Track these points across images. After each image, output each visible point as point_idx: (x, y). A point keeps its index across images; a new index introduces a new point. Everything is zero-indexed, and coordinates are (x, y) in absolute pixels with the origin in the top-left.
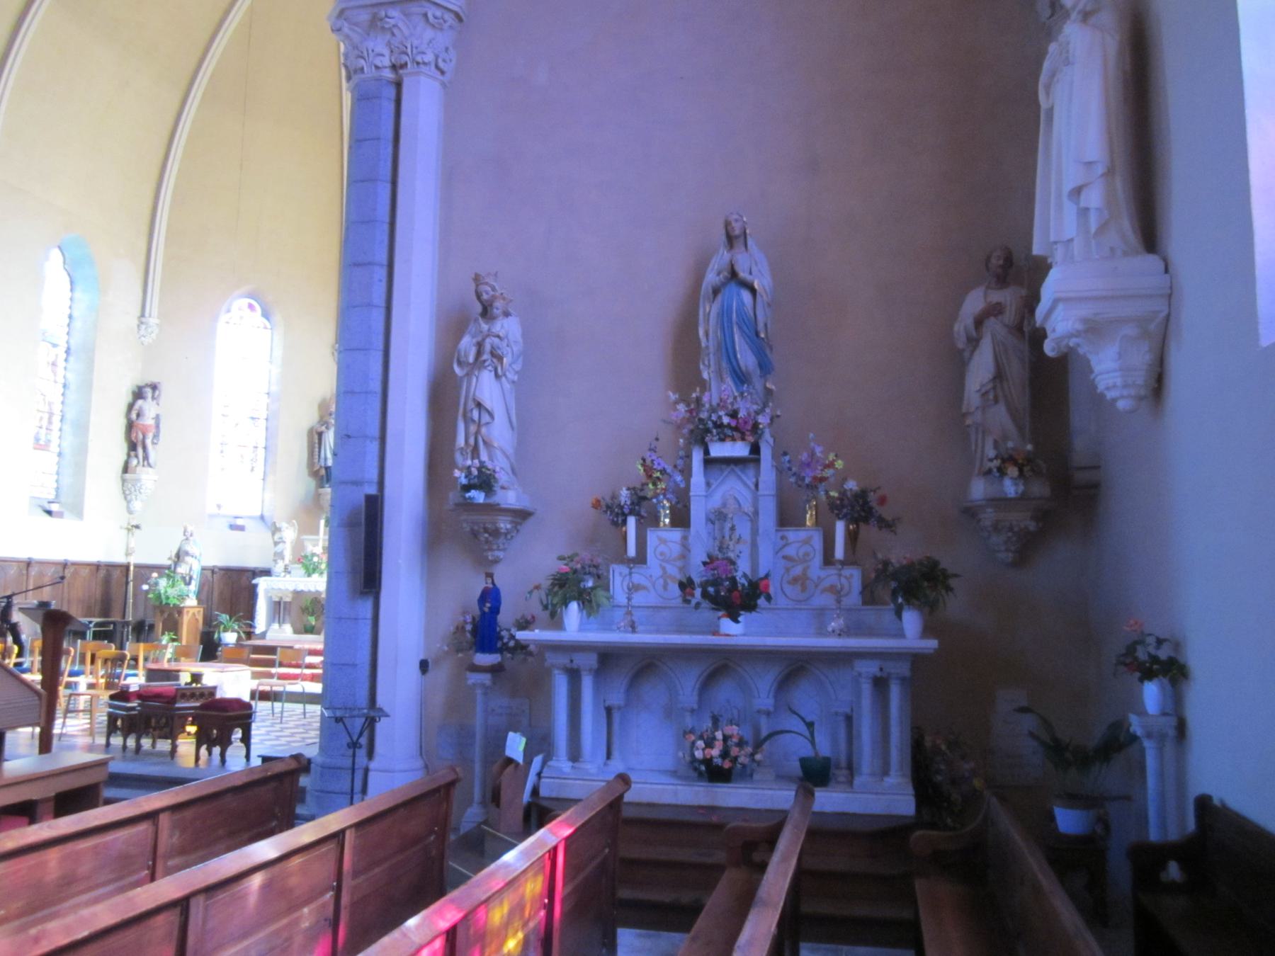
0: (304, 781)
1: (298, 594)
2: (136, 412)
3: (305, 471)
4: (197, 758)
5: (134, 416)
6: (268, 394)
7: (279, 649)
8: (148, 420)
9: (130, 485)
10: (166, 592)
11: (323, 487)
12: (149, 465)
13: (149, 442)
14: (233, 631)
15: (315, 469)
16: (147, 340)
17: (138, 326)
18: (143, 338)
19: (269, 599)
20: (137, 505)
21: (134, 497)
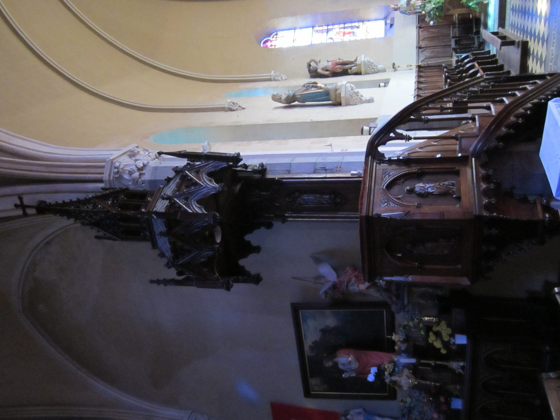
2: (324, 71)
5: (327, 73)
6: (313, 27)
12: (356, 60)
17: (276, 81)
20: (380, 66)
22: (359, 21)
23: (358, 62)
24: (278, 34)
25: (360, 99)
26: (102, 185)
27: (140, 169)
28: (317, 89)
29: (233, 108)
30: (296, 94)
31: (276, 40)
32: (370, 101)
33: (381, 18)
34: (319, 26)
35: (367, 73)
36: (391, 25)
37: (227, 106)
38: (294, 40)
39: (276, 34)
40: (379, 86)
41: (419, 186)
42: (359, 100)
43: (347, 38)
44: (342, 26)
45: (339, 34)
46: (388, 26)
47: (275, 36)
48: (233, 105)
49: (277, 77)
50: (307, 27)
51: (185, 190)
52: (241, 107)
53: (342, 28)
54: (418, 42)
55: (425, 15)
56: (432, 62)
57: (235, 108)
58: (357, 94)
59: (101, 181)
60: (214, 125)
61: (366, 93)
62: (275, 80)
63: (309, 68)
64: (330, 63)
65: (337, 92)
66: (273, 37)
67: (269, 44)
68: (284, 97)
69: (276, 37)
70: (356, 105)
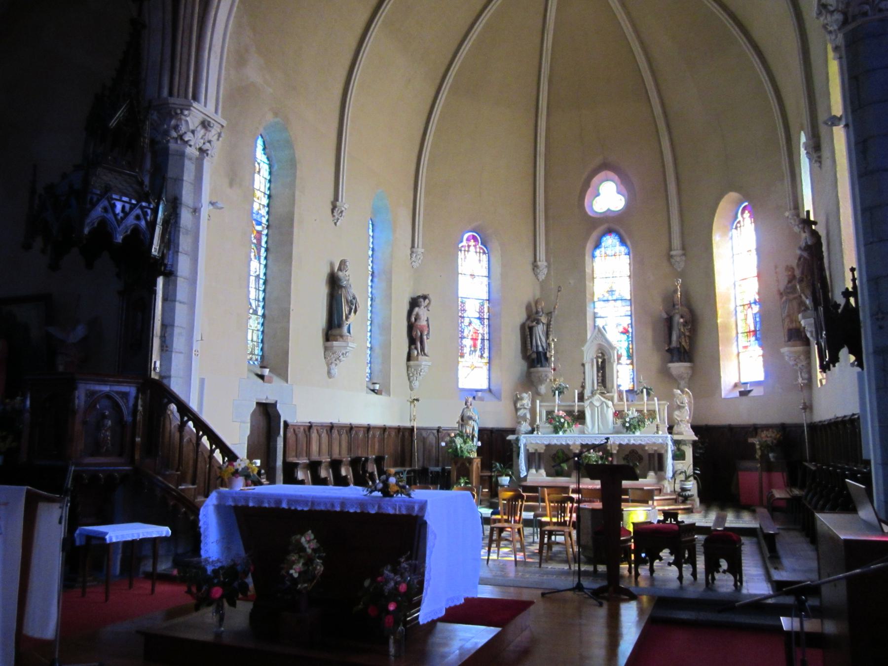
1: (548, 446)
4: (680, 578)
5: (413, 319)
6: (488, 300)
7: (630, 490)
8: (423, 322)
9: (413, 370)
10: (461, 447)
11: (534, 367)
12: (425, 354)
13: (425, 337)
14: (507, 475)
15: (528, 354)
16: (416, 265)
17: (411, 254)
18: (413, 263)
19: (527, 451)
20: (416, 384)
21: (415, 378)
22: (490, 358)
24: (484, 255)
25: (332, 363)
27: (181, 137)
28: (346, 314)
29: (335, 212)
30: (344, 290)
31: (476, 252)
33: (491, 385)
34: (489, 308)
37: (338, 204)
38: (473, 275)
39: (484, 253)
42: (330, 361)
43: (468, 342)
44: (486, 337)
45: (475, 333)
47: (482, 251)
48: (339, 211)
49: (415, 255)
52: (337, 221)
53: (484, 337)
57: (335, 214)
59: (171, 94)
60: (297, 193)
63: (422, 297)
65: (339, 337)
66: (481, 248)
69: (480, 253)
70: (325, 358)
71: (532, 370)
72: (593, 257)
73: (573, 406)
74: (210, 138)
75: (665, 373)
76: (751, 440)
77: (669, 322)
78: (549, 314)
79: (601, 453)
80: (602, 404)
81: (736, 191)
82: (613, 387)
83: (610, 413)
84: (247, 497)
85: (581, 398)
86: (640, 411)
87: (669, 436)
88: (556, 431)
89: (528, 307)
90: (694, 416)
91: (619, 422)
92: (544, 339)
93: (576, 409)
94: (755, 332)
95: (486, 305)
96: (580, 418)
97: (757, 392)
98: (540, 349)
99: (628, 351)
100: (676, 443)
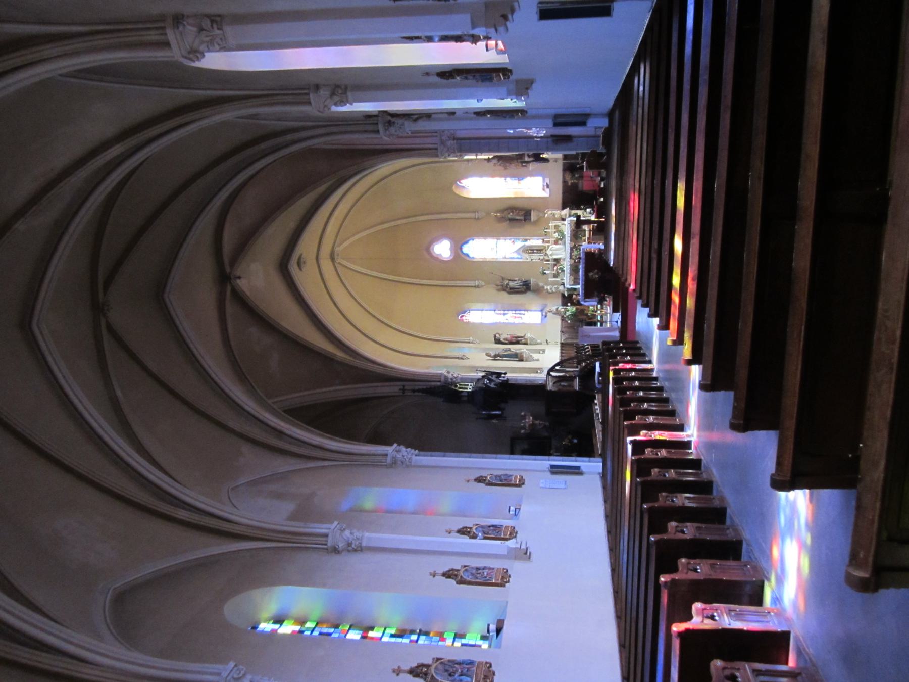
0: (656, 321)
3: (524, 295)
20: (539, 341)
22: (524, 311)
23: (526, 338)
26: (439, 384)
27: (455, 378)
32: (538, 360)
34: (499, 311)
35: (531, 344)
36: (546, 316)
37: (460, 356)
39: (469, 312)
40: (540, 353)
41: (562, 384)
43: (517, 321)
44: (514, 312)
46: (544, 317)
50: (490, 310)
51: (621, 345)
54: (562, 329)
55: (565, 318)
56: (569, 341)
58: (531, 356)
61: (535, 356)
62: (472, 343)
64: (509, 336)
67: (464, 318)
68: (493, 355)
71: (532, 289)
72: (473, 258)
73: (552, 264)
74: (401, 456)
75: (536, 222)
76: (569, 184)
77: (511, 220)
78: (503, 279)
79: (574, 249)
80: (551, 250)
81: (452, 187)
82: (543, 246)
83: (555, 247)
84: (582, 285)
85: (548, 260)
86: (555, 233)
87: (567, 219)
88: (563, 271)
89: (499, 290)
90: (558, 209)
91: (560, 242)
92: (516, 282)
93: (554, 263)
94: (519, 180)
95: (497, 312)
96: (557, 261)
97: (547, 180)
98: (521, 284)
99: (523, 242)
100: (570, 216)
